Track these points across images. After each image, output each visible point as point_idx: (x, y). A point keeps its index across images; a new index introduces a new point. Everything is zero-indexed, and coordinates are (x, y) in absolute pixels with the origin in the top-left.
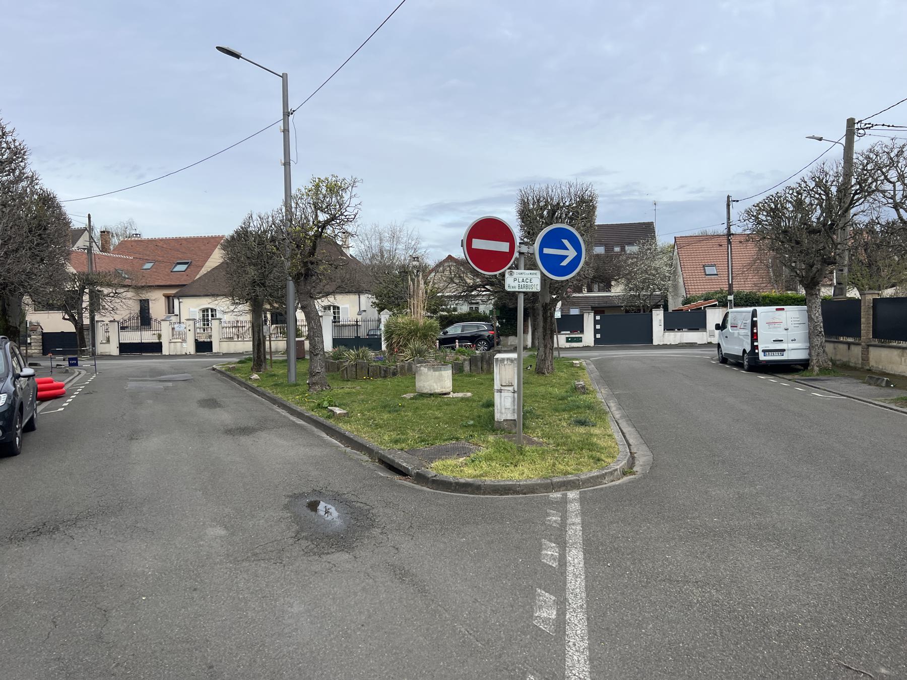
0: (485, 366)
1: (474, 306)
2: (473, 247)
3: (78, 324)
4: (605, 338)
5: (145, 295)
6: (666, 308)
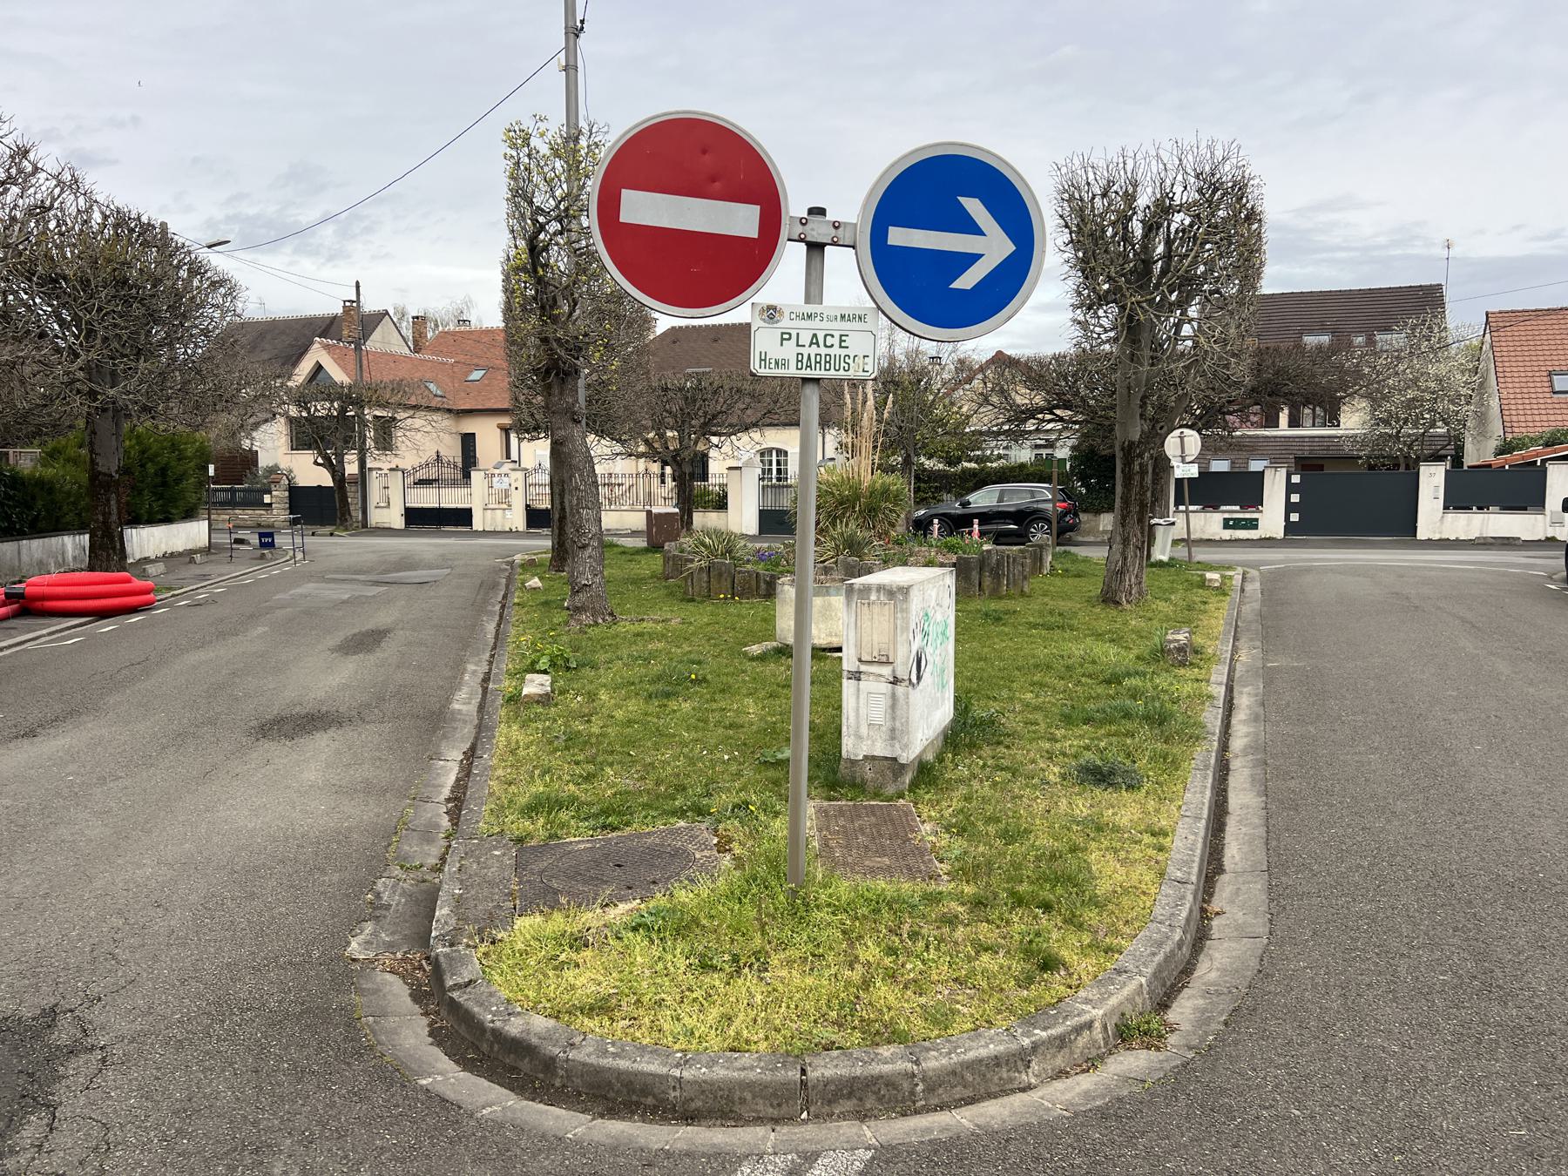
0: (987, 581)
1: (1044, 452)
2: (624, 218)
3: (336, 471)
4: (1311, 521)
5: (469, 426)
6: (1457, 461)
